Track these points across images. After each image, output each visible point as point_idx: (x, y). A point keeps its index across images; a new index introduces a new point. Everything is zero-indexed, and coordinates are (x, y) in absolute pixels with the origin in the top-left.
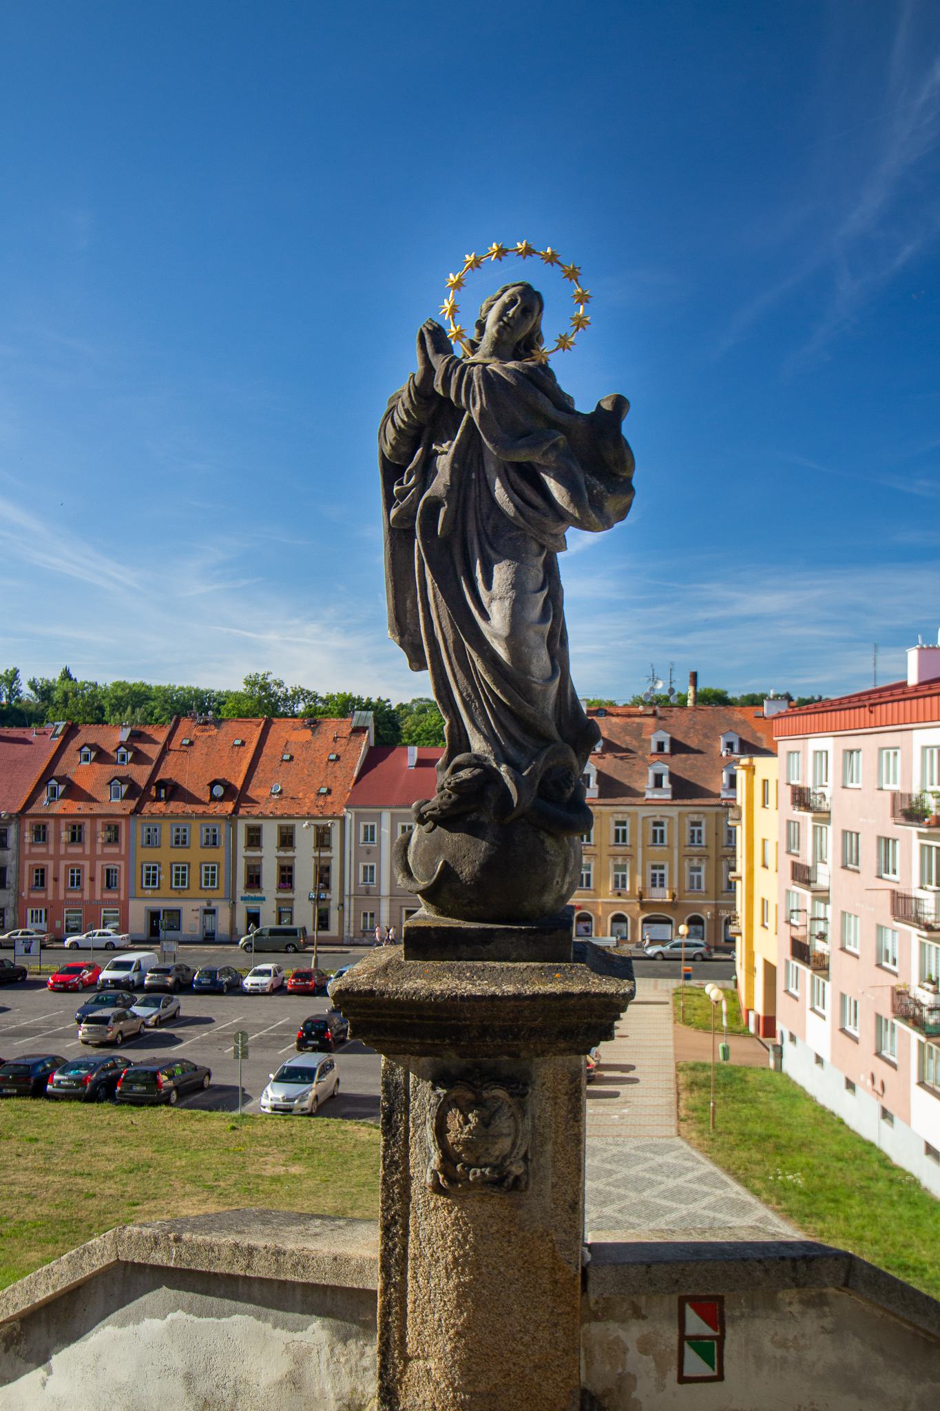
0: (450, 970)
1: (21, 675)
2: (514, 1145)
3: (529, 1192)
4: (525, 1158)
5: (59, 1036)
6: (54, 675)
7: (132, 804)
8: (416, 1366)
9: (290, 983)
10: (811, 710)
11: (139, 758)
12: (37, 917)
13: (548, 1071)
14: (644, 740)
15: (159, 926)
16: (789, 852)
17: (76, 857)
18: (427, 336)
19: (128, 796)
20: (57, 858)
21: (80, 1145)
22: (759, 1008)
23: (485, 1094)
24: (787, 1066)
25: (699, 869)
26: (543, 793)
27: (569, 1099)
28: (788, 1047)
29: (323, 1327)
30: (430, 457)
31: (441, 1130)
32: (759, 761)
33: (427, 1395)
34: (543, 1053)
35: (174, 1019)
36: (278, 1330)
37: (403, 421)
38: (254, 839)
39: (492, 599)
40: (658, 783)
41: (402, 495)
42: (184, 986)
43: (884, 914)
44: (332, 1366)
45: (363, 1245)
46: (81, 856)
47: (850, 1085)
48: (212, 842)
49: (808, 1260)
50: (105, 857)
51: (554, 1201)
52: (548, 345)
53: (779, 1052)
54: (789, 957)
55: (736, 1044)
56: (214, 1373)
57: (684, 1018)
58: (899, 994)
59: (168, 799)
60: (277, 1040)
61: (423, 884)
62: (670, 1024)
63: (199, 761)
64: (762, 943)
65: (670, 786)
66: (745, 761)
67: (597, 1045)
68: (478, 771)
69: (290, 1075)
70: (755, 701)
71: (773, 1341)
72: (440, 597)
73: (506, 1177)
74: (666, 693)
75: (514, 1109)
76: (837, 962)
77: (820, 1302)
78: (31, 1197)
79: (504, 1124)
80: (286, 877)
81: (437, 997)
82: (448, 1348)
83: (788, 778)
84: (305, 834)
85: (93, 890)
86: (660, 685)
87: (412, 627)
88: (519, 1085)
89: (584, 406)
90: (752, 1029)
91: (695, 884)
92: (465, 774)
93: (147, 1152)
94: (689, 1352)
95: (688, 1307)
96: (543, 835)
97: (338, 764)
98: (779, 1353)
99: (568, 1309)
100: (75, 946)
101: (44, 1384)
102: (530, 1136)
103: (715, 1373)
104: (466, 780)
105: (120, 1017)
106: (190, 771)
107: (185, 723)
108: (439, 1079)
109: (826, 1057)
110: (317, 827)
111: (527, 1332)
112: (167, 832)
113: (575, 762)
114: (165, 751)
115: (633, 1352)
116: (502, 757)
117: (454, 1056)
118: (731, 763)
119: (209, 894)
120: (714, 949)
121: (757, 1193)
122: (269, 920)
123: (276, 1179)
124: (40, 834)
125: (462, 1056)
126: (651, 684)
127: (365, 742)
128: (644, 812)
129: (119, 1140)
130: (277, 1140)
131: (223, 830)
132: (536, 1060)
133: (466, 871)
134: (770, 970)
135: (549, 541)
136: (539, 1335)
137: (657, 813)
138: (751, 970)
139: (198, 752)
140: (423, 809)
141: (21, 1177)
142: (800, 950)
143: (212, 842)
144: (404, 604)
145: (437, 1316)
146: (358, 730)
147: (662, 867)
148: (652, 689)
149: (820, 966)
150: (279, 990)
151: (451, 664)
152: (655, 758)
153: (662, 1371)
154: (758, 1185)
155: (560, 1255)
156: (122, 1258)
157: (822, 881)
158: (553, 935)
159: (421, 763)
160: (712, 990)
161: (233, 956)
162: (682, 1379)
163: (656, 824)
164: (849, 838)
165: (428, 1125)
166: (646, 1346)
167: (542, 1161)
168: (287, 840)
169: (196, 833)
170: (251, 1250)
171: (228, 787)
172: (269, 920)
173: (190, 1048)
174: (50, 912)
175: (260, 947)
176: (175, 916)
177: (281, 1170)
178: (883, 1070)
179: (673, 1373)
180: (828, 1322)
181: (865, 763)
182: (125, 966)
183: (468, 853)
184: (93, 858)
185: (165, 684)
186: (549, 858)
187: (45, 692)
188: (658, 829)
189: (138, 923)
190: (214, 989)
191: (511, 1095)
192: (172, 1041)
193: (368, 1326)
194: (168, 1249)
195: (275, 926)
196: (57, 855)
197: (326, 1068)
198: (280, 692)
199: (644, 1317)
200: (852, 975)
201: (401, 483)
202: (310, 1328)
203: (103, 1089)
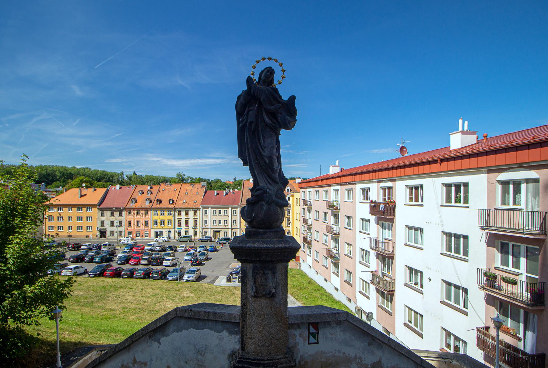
1: (124, 173)
17: (139, 218)
49: (338, 313)
52: (276, 82)
58: (328, 250)
80: (187, 222)
93: (157, 291)
94: (311, 336)
95: (310, 326)
96: (277, 207)
98: (331, 336)
115: (298, 337)
119: (170, 227)
121: (296, 299)
123: (187, 297)
129: (151, 288)
130: (188, 288)
139: (166, 192)
141: (129, 298)
146: (203, 186)
154: (297, 297)
162: (309, 343)
166: (301, 335)
170: (209, 313)
177: (189, 295)
179: (307, 342)
180: (342, 329)
187: (130, 179)
194: (189, 313)
195: (184, 235)
197: (198, 270)
198: (185, 177)
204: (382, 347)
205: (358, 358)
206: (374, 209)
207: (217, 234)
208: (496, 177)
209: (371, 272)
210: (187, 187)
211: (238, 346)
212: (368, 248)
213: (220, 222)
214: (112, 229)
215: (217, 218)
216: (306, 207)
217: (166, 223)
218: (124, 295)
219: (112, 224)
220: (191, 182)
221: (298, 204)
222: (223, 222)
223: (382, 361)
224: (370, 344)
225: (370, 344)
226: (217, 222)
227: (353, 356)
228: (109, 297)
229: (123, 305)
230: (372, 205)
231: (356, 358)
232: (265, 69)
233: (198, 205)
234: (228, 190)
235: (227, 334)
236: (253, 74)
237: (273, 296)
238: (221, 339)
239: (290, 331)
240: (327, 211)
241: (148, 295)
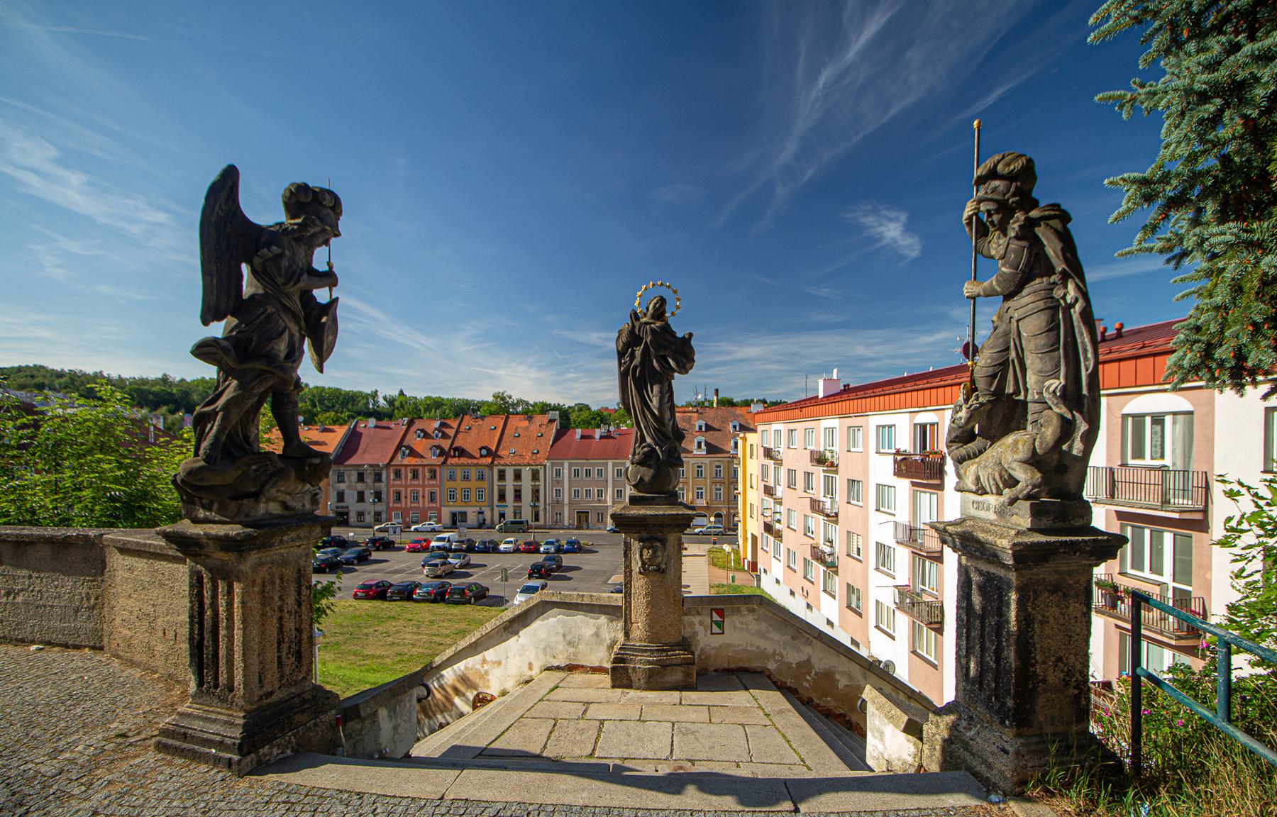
5: (414, 573)
6: (395, 393)
7: (442, 459)
9: (522, 547)
10: (775, 408)
11: (445, 436)
12: (397, 516)
13: (672, 538)
15: (457, 520)
19: (440, 455)
20: (406, 486)
21: (432, 622)
22: (749, 558)
24: (762, 585)
26: (669, 455)
28: (763, 575)
30: (633, 351)
31: (641, 555)
32: (749, 435)
35: (468, 565)
38: (502, 476)
42: (471, 549)
43: (808, 511)
46: (418, 486)
47: (792, 593)
48: (481, 478)
50: (430, 486)
53: (759, 579)
55: (738, 575)
57: (713, 563)
59: (459, 457)
60: (519, 575)
63: (475, 436)
64: (752, 526)
69: (527, 590)
70: (747, 403)
76: (786, 534)
77: (753, 610)
78: (414, 645)
79: (659, 553)
80: (518, 495)
83: (1123, 455)
84: (526, 473)
85: (424, 503)
88: (664, 542)
89: (679, 335)
91: (718, 496)
100: (416, 530)
105: (444, 564)
106: (469, 442)
107: (467, 418)
108: (640, 540)
109: (781, 579)
112: (459, 473)
114: (457, 432)
116: (657, 444)
118: (735, 436)
120: (728, 529)
122: (510, 517)
124: (398, 474)
127: (555, 426)
128: (692, 461)
131: (486, 472)
133: (647, 479)
134: (754, 538)
138: (745, 539)
139: (473, 432)
142: (768, 528)
143: (481, 478)
146: (551, 421)
149: (778, 535)
150: (517, 551)
153: (706, 630)
157: (779, 494)
158: (672, 498)
159: (583, 437)
160: (727, 548)
161: (493, 535)
164: (792, 473)
168: (518, 476)
169: (474, 473)
171: (489, 450)
172: (510, 517)
173: (477, 577)
174: (404, 513)
175: (506, 530)
176: (464, 514)
178: (807, 585)
181: (798, 436)
182: (442, 539)
183: (647, 473)
184: (424, 486)
185: (451, 397)
187: (391, 402)
189: (446, 518)
190: (485, 550)
192: (468, 575)
193: (619, 618)
196: (406, 484)
200: (793, 540)
203: (440, 596)
206: (904, 466)
207: (583, 519)
208: (1122, 407)
209: (896, 587)
211: (621, 636)
212: (889, 541)
214: (360, 507)
216: (771, 463)
217: (474, 495)
218: (398, 632)
219: (361, 497)
220: (526, 412)
223: (813, 660)
224: (794, 638)
225: (794, 638)
228: (367, 635)
229: (396, 649)
230: (899, 458)
231: (774, 653)
237: (663, 571)
240: (811, 469)
241: (443, 631)
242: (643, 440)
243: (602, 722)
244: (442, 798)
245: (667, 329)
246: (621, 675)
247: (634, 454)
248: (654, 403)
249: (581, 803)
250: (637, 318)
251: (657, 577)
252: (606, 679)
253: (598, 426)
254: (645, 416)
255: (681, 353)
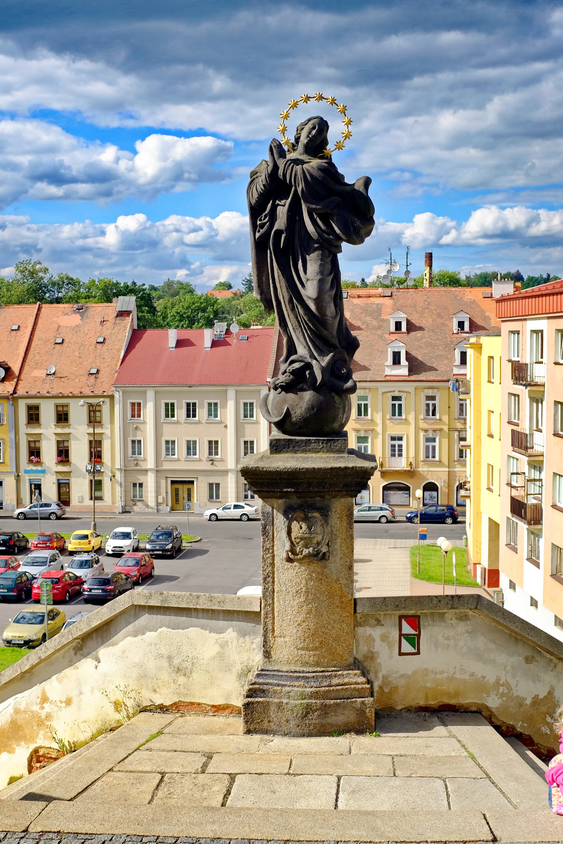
0: (293, 458)
2: (323, 538)
3: (329, 561)
4: (328, 544)
8: (280, 640)
14: (383, 320)
16: (509, 422)
18: (274, 149)
22: (485, 563)
23: (309, 515)
25: (434, 440)
27: (348, 518)
29: (233, 631)
31: (289, 532)
32: (485, 340)
33: (285, 653)
34: (335, 497)
36: (212, 634)
37: (262, 189)
38: (34, 416)
39: (308, 280)
40: (396, 360)
41: (262, 226)
44: (238, 649)
45: (253, 592)
51: (341, 565)
54: (510, 515)
56: (182, 655)
61: (277, 419)
62: (408, 577)
64: (487, 506)
65: (407, 363)
66: (473, 340)
67: (360, 492)
68: (302, 364)
71: (443, 637)
72: (281, 277)
73: (320, 553)
74: (403, 276)
75: (322, 522)
80: (63, 454)
81: (288, 469)
82: (295, 631)
83: (509, 354)
84: (78, 411)
86: (397, 268)
87: (266, 290)
88: (325, 512)
90: (479, 580)
92: (297, 365)
94: (404, 641)
95: (403, 620)
96: (333, 394)
97: (105, 347)
99: (348, 614)
101: (96, 667)
102: (330, 535)
103: (416, 651)
104: (297, 369)
110: (90, 405)
111: (330, 624)
113: (347, 358)
115: (378, 641)
117: (295, 498)
125: (299, 498)
126: (388, 267)
127: (129, 323)
132: (332, 500)
134: (494, 526)
135: (333, 249)
136: (335, 625)
137: (396, 389)
140: (277, 382)
142: (518, 507)
144: (262, 279)
145: (289, 617)
146: (122, 314)
147: (400, 439)
148: (389, 271)
151: (303, 323)
152: (393, 337)
155: (344, 590)
156: (135, 603)
159: (180, 343)
160: (443, 543)
162: (401, 654)
163: (394, 398)
165: (283, 530)
166: (384, 638)
167: (335, 546)
168: (62, 417)
180: (469, 628)
186: (336, 405)
188: (397, 403)
191: (321, 515)
193: (259, 623)
199: (383, 625)
201: (260, 220)
202: (227, 632)
204: (555, 666)
205: (503, 685)
207: (183, 493)
210: (60, 317)
211: (258, 658)
213: (191, 447)
215: (180, 430)
216: (523, 392)
221: (496, 380)
222: (202, 450)
224: (528, 660)
225: (528, 660)
226: (181, 449)
227: (491, 679)
231: (498, 683)
232: (309, 120)
233: (105, 384)
234: (220, 327)
235: (234, 634)
236: (284, 131)
238: (224, 645)
239: (360, 630)
242: (292, 349)
243: (232, 777)
244: (26, 831)
245: (330, 172)
246: (256, 713)
247: (275, 374)
248: (309, 291)
249: (211, 835)
250: (282, 154)
251: (316, 566)
252: (239, 723)
253: (210, 324)
254: (293, 309)
255: (348, 210)
